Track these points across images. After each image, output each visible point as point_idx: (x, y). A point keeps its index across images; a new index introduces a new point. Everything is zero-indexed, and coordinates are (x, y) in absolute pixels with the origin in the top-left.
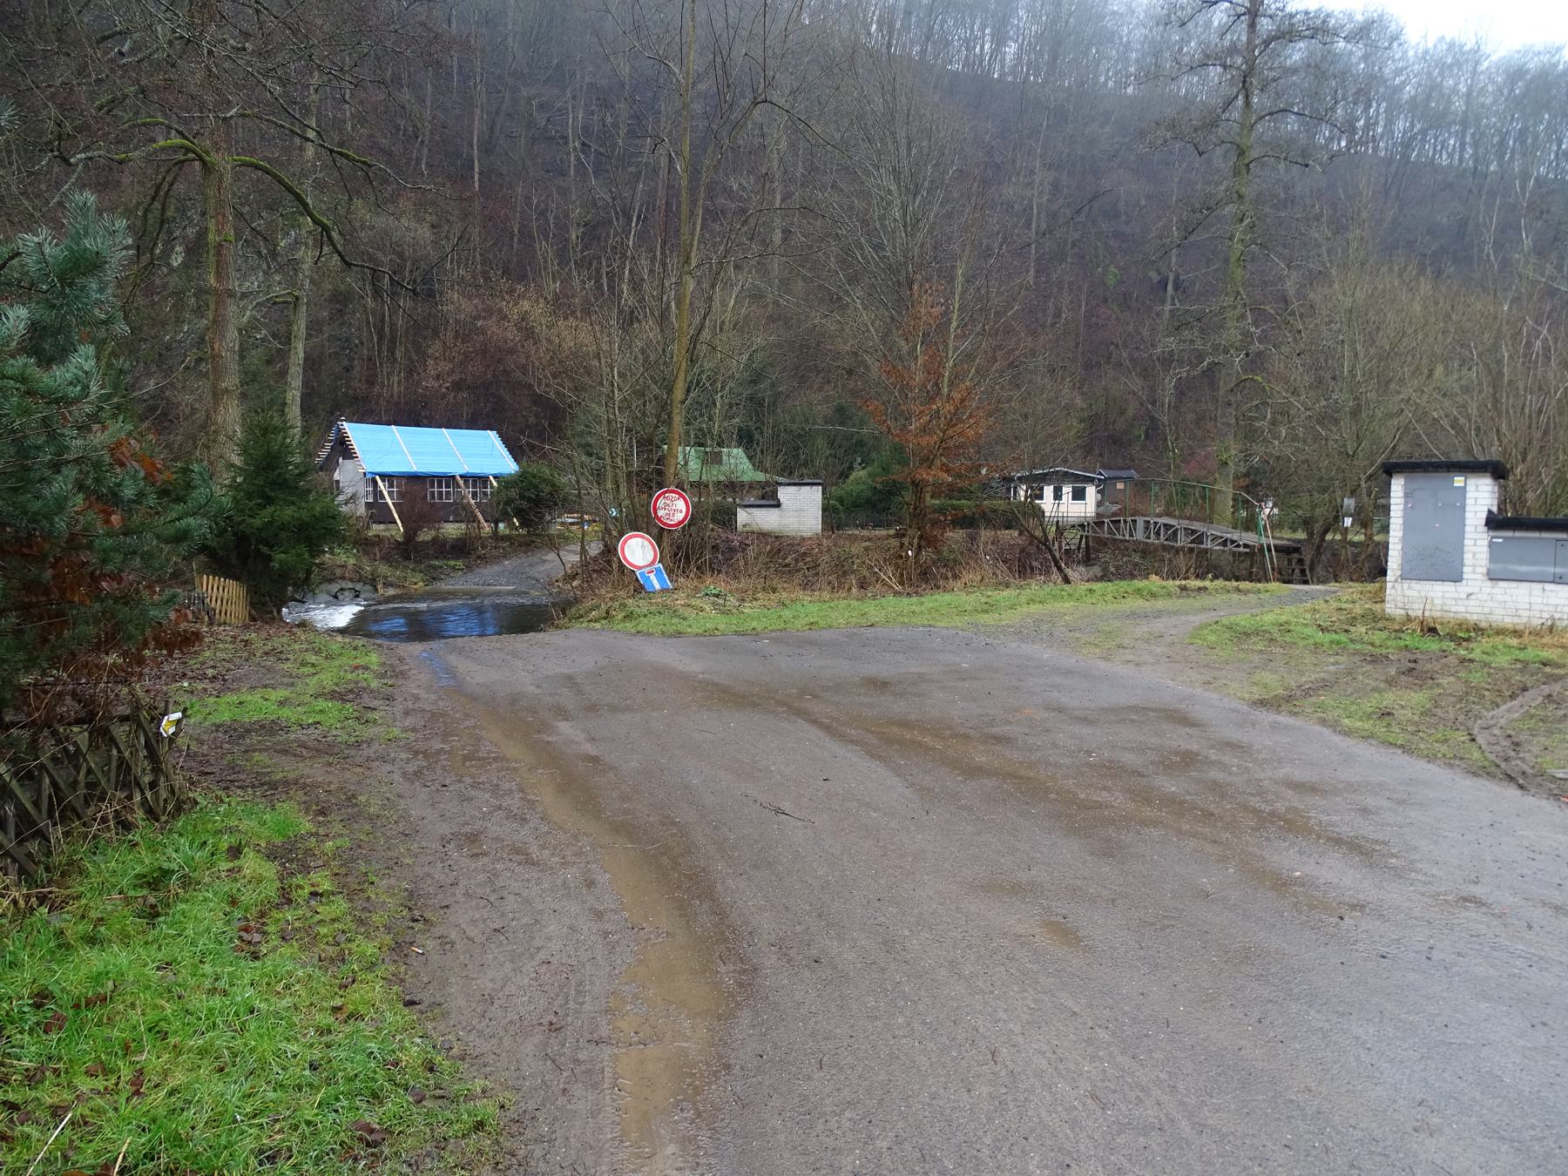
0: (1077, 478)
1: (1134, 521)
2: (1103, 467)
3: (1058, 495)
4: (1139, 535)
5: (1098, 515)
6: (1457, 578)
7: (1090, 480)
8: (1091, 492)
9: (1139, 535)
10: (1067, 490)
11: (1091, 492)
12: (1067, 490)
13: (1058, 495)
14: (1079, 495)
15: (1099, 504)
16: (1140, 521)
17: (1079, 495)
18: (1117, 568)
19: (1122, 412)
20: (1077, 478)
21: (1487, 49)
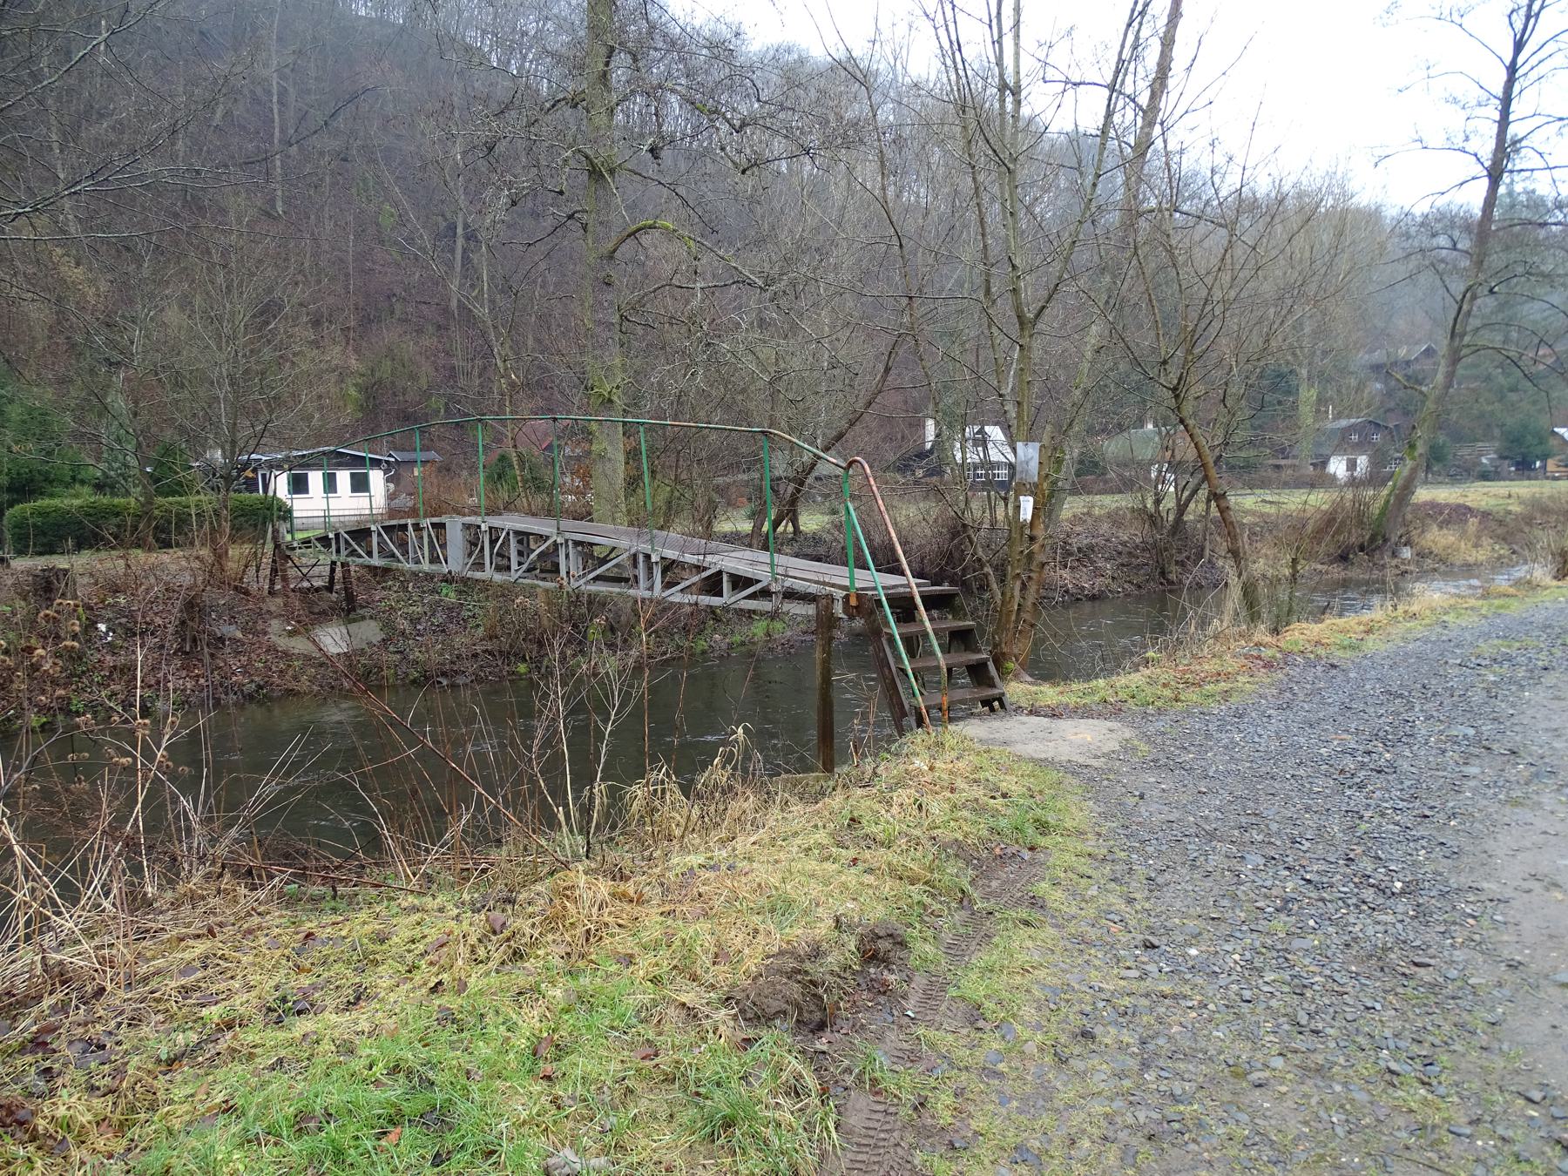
0: (358, 461)
1: (440, 527)
2: (395, 449)
3: (330, 485)
4: (456, 560)
5: (392, 512)
6: (354, 490)
7: (376, 463)
8: (376, 478)
9: (456, 560)
10: (343, 477)
11: (376, 478)
12: (343, 477)
13: (330, 485)
14: (360, 484)
15: (391, 497)
16: (455, 528)
17: (360, 484)
18: (414, 621)
19: (413, 377)
20: (358, 461)
21: (749, 32)
